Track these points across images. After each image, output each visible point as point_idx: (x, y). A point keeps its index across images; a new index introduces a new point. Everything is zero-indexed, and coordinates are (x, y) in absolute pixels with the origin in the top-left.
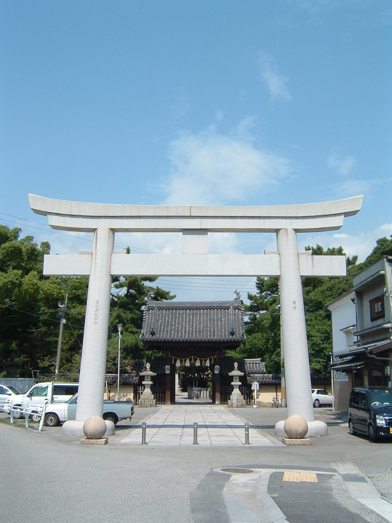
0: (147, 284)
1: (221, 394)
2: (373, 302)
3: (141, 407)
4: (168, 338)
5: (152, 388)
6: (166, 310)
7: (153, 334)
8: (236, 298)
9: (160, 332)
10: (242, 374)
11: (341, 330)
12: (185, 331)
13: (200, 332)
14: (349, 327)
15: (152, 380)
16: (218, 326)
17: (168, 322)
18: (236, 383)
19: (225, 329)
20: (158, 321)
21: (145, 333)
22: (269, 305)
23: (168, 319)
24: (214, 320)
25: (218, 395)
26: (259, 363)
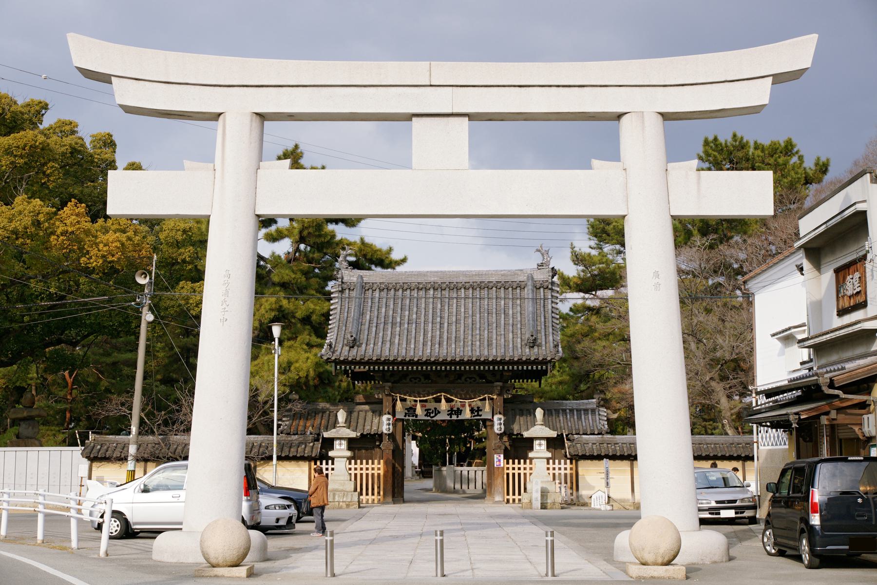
0: (341, 232)
2: (841, 272)
6: (381, 290)
7: (354, 344)
8: (540, 262)
10: (554, 434)
11: (773, 335)
14: (789, 329)
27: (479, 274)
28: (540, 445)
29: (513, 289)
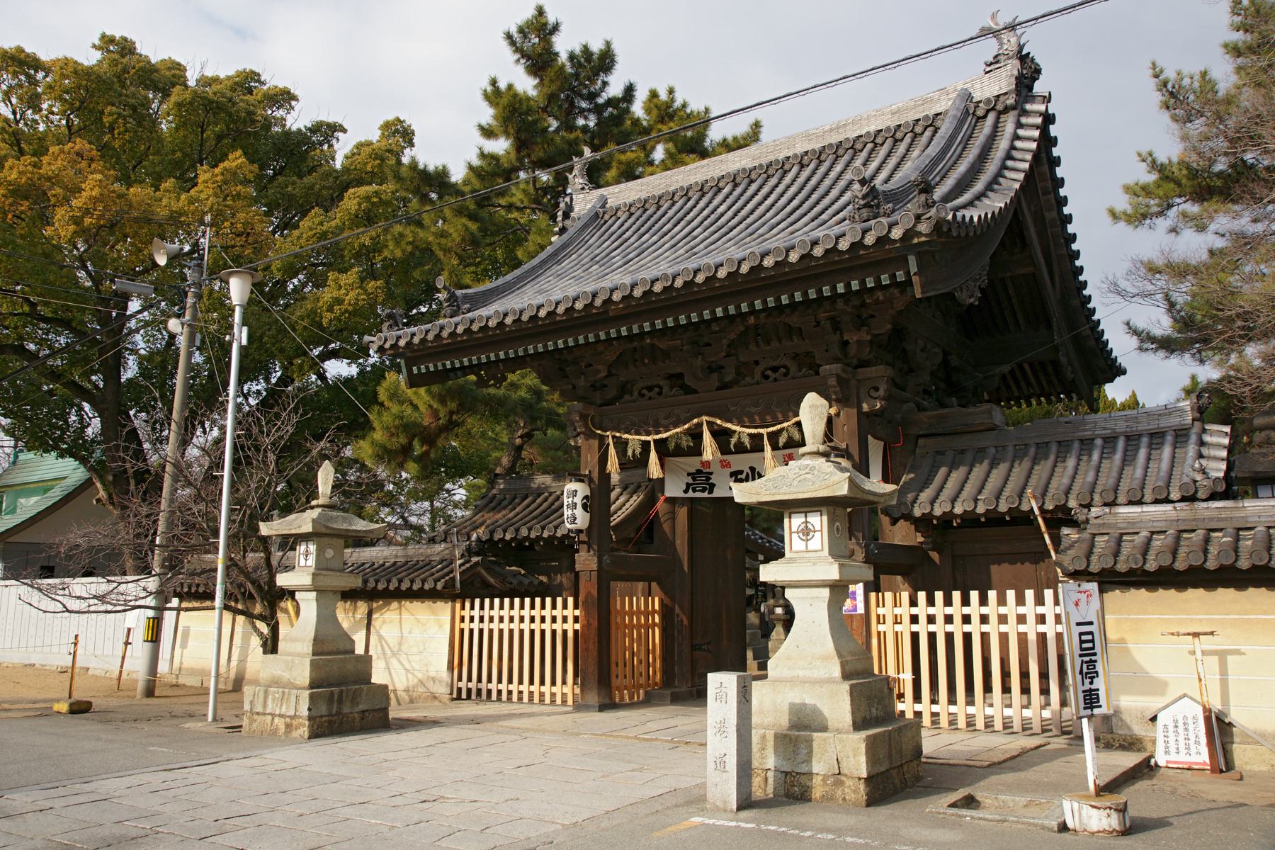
28: (806, 532)
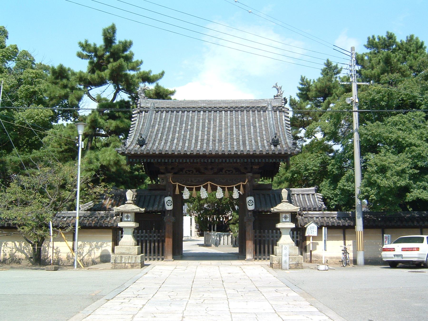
1: (255, 243)
3: (114, 268)
4: (167, 148)
5: (137, 234)
9: (155, 141)
12: (196, 141)
13: (220, 141)
15: (136, 221)
16: (249, 133)
17: (169, 128)
18: (285, 225)
19: (262, 138)
20: (153, 126)
21: (131, 144)
22: (317, 115)
23: (170, 124)
24: (243, 126)
25: (250, 245)
26: (313, 195)
27: (234, 102)
29: (258, 111)
